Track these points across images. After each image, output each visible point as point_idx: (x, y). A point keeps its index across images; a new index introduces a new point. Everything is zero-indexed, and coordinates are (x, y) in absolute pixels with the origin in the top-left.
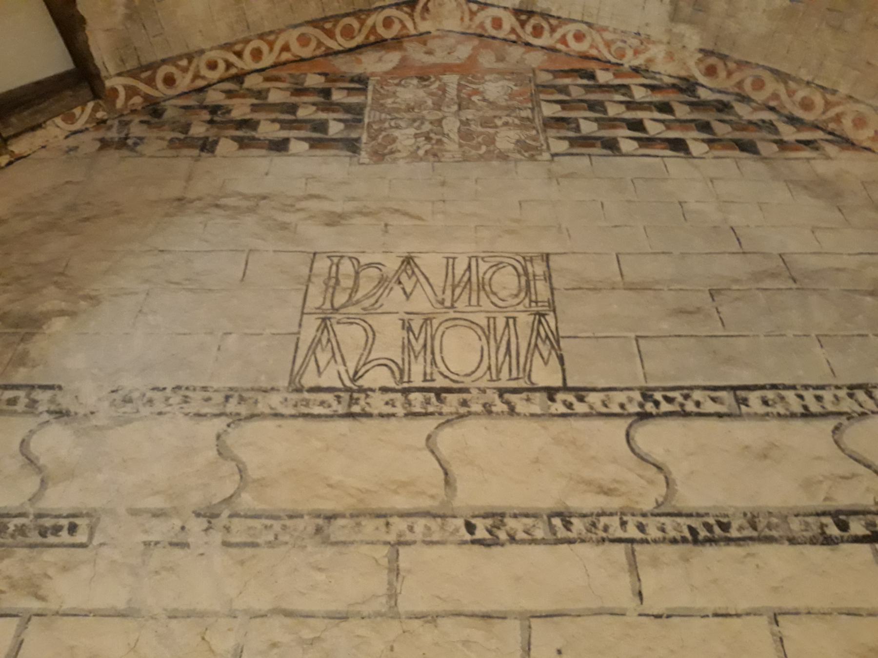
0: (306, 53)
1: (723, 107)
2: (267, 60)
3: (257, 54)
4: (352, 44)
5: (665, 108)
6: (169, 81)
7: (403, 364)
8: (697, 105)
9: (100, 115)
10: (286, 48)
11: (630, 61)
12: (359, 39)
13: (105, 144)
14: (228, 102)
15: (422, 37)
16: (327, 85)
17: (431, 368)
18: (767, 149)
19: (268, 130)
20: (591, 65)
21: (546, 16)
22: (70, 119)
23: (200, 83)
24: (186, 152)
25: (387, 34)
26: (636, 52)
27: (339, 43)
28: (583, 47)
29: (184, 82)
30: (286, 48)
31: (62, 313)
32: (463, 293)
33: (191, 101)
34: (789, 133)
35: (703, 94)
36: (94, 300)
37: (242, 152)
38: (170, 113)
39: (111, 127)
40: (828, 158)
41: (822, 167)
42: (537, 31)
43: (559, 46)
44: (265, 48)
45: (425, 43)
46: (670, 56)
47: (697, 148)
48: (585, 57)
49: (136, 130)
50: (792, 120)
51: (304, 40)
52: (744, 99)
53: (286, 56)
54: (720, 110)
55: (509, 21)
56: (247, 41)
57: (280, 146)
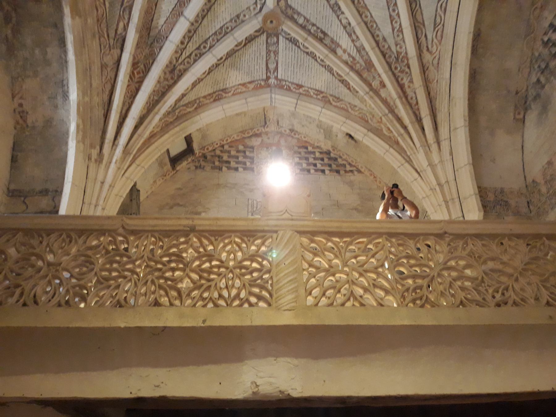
0: (238, 138)
1: (336, 159)
2: (229, 141)
3: (227, 140)
4: (249, 135)
5: (322, 159)
6: (208, 149)
7: (26, 213)
8: (330, 159)
9: (193, 159)
10: (234, 138)
11: (316, 144)
12: (251, 134)
13: (196, 167)
14: (221, 154)
15: (267, 133)
16: (245, 149)
17: (177, 67)
18: (342, 172)
19: (233, 164)
20: (307, 144)
21: (297, 132)
22: (187, 160)
23: (214, 148)
24: (216, 170)
25: (258, 132)
26: (318, 143)
27: (246, 135)
28: (306, 139)
29: (210, 149)
30: (234, 138)
31: (204, 212)
32: (327, 76)
33: (213, 154)
34: (348, 168)
35: (332, 155)
36: (209, 209)
37: (228, 171)
38: (209, 157)
39: (196, 162)
40: (354, 175)
41: (352, 178)
42: (295, 134)
43: (300, 138)
44: (229, 139)
45: (267, 135)
46: (325, 145)
47: (327, 172)
48: (306, 142)
49: (203, 163)
50: (350, 164)
51: (238, 136)
52: (340, 157)
53: (233, 140)
54: (335, 161)
55: (288, 131)
56: (225, 138)
57: (236, 169)
